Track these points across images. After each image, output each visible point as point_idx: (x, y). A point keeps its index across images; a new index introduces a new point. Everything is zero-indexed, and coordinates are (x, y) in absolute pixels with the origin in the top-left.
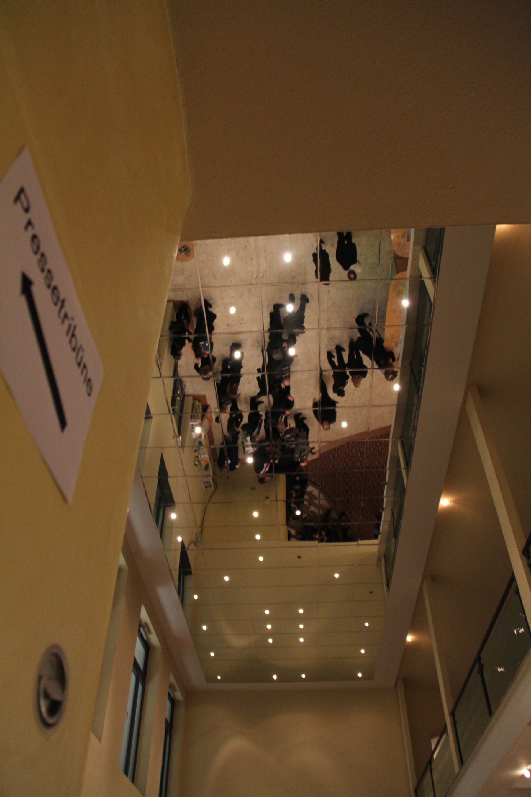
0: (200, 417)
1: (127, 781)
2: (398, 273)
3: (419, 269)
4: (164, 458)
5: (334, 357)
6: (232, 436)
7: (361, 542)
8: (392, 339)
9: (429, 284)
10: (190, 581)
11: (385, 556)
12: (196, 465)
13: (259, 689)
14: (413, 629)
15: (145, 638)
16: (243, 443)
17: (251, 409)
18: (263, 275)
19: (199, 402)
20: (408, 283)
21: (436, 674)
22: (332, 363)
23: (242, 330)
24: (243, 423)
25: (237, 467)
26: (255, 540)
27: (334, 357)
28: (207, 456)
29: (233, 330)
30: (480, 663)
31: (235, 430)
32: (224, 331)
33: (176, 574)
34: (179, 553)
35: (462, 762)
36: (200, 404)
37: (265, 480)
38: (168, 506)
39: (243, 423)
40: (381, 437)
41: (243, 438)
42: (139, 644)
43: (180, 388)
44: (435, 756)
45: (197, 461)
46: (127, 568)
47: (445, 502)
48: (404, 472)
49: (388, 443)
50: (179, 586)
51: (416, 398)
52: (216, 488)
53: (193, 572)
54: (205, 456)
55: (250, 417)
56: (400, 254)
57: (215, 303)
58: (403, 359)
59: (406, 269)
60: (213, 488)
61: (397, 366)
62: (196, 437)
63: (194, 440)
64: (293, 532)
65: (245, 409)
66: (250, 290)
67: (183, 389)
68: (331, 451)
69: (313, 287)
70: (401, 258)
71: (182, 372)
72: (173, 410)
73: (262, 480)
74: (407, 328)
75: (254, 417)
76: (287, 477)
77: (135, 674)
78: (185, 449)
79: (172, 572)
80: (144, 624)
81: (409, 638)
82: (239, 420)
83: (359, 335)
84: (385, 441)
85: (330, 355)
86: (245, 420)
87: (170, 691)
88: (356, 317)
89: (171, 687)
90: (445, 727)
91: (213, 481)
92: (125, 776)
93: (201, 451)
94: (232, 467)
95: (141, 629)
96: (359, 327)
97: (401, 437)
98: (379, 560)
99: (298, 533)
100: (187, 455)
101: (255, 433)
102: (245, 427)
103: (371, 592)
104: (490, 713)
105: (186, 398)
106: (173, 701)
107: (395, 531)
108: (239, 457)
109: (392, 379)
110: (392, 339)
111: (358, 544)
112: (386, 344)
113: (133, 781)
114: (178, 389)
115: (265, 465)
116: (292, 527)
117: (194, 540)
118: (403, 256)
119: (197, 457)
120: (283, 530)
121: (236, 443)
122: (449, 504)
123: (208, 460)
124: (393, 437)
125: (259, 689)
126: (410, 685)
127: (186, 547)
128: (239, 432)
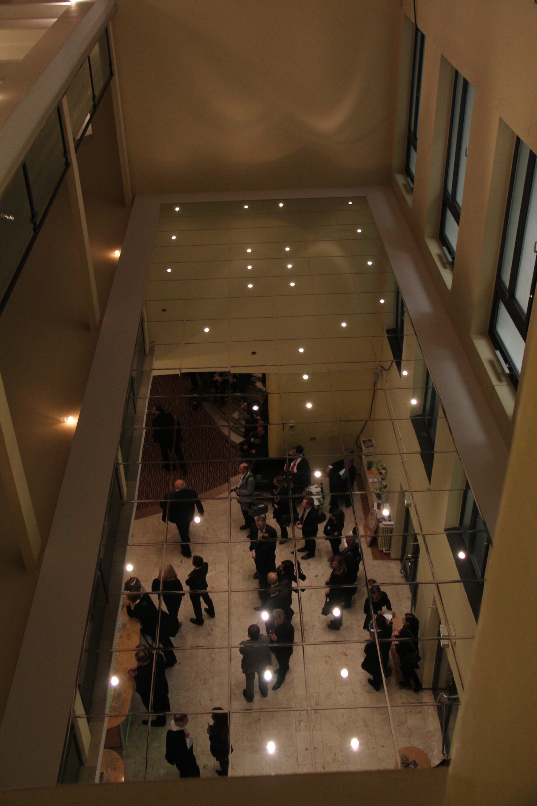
0: (380, 533)
1: (464, 73)
2: (118, 727)
3: (91, 731)
4: (426, 477)
5: (205, 610)
6: (337, 507)
7: (178, 372)
8: (130, 634)
9: (79, 708)
10: (389, 321)
11: (145, 356)
12: (384, 468)
13: (301, 191)
14: (113, 265)
15: (445, 248)
16: (323, 497)
17: (314, 541)
18: (300, 724)
19: (382, 551)
20: (107, 711)
21: (86, 213)
22: (209, 601)
23: (328, 647)
24: (325, 523)
25: (331, 467)
26: (308, 373)
27: (205, 610)
28: (370, 480)
29: (340, 647)
30: (35, 224)
31: (334, 515)
32: (353, 645)
33: (408, 330)
34: (404, 357)
35: (59, 110)
36: (380, 549)
37: (295, 450)
38: (419, 416)
39: (325, 523)
40: (146, 505)
41: (323, 504)
42: (453, 240)
43: (408, 570)
44: (88, 117)
45: (383, 473)
46: (473, 336)
47: (71, 421)
48: (120, 460)
49: (139, 497)
50: (403, 314)
51: (101, 557)
52: (358, 439)
53: (385, 334)
54: (372, 480)
55: (315, 531)
56: (115, 754)
57: (364, 685)
58: (118, 606)
59: (108, 730)
60: (362, 439)
61: (123, 600)
62: (385, 504)
63: (387, 501)
64: (259, 385)
65: (322, 543)
66: (317, 704)
67: (404, 568)
68: (210, 488)
69: (235, 707)
70: (112, 748)
71: (406, 591)
72: (416, 540)
73: (300, 450)
74: (111, 648)
75: (309, 531)
76: (267, 455)
77: (456, 202)
78: (399, 489)
79: (414, 333)
80: (448, 266)
81: (117, 254)
82: (329, 528)
83: (172, 639)
84: (142, 499)
85: (211, 612)
86: (321, 527)
87: (412, 186)
88: (176, 664)
89: (410, 190)
90: (76, 148)
91: (361, 449)
92: (467, 79)
93: (378, 486)
94: (338, 466)
95: (450, 260)
96: (171, 649)
97: (123, 505)
98: (152, 350)
99: (253, 383)
100: (397, 479)
101: (308, 511)
102: (322, 518)
103: (164, 310)
104: (24, 167)
105: (399, 556)
106: (407, 172)
107: (133, 386)
108: (328, 479)
109: (132, 579)
110: (130, 634)
111: (180, 369)
112: (138, 627)
113: (457, 73)
114: (411, 568)
115: (295, 470)
116: (260, 390)
117: (384, 373)
118: (111, 751)
119: (382, 479)
120: (272, 386)
121: (332, 497)
122: (65, 419)
123: (368, 475)
124: (133, 503)
125: (301, 191)
126: (117, 198)
127: (394, 365)
128: (330, 512)
